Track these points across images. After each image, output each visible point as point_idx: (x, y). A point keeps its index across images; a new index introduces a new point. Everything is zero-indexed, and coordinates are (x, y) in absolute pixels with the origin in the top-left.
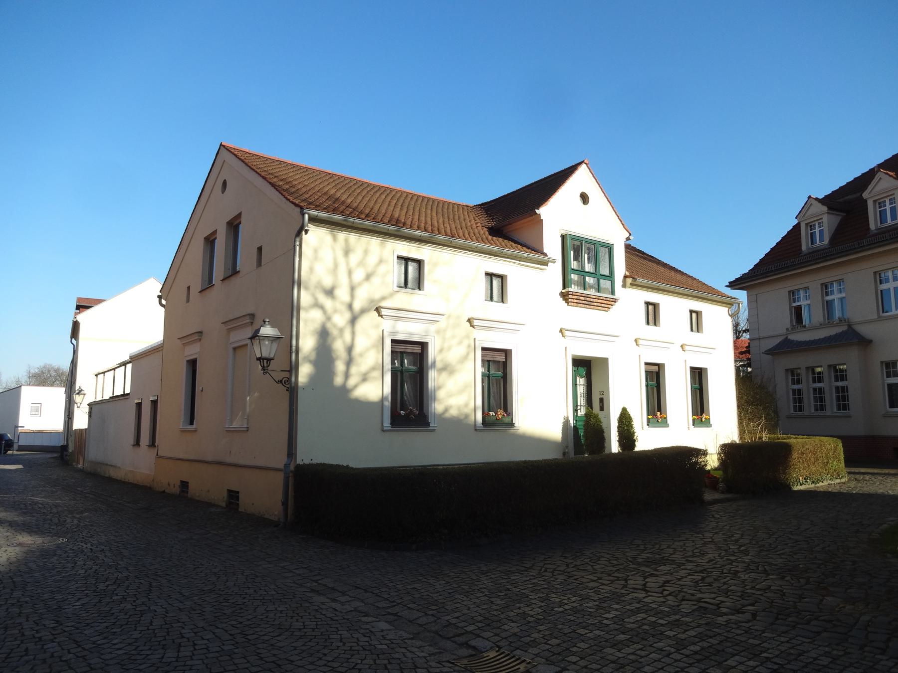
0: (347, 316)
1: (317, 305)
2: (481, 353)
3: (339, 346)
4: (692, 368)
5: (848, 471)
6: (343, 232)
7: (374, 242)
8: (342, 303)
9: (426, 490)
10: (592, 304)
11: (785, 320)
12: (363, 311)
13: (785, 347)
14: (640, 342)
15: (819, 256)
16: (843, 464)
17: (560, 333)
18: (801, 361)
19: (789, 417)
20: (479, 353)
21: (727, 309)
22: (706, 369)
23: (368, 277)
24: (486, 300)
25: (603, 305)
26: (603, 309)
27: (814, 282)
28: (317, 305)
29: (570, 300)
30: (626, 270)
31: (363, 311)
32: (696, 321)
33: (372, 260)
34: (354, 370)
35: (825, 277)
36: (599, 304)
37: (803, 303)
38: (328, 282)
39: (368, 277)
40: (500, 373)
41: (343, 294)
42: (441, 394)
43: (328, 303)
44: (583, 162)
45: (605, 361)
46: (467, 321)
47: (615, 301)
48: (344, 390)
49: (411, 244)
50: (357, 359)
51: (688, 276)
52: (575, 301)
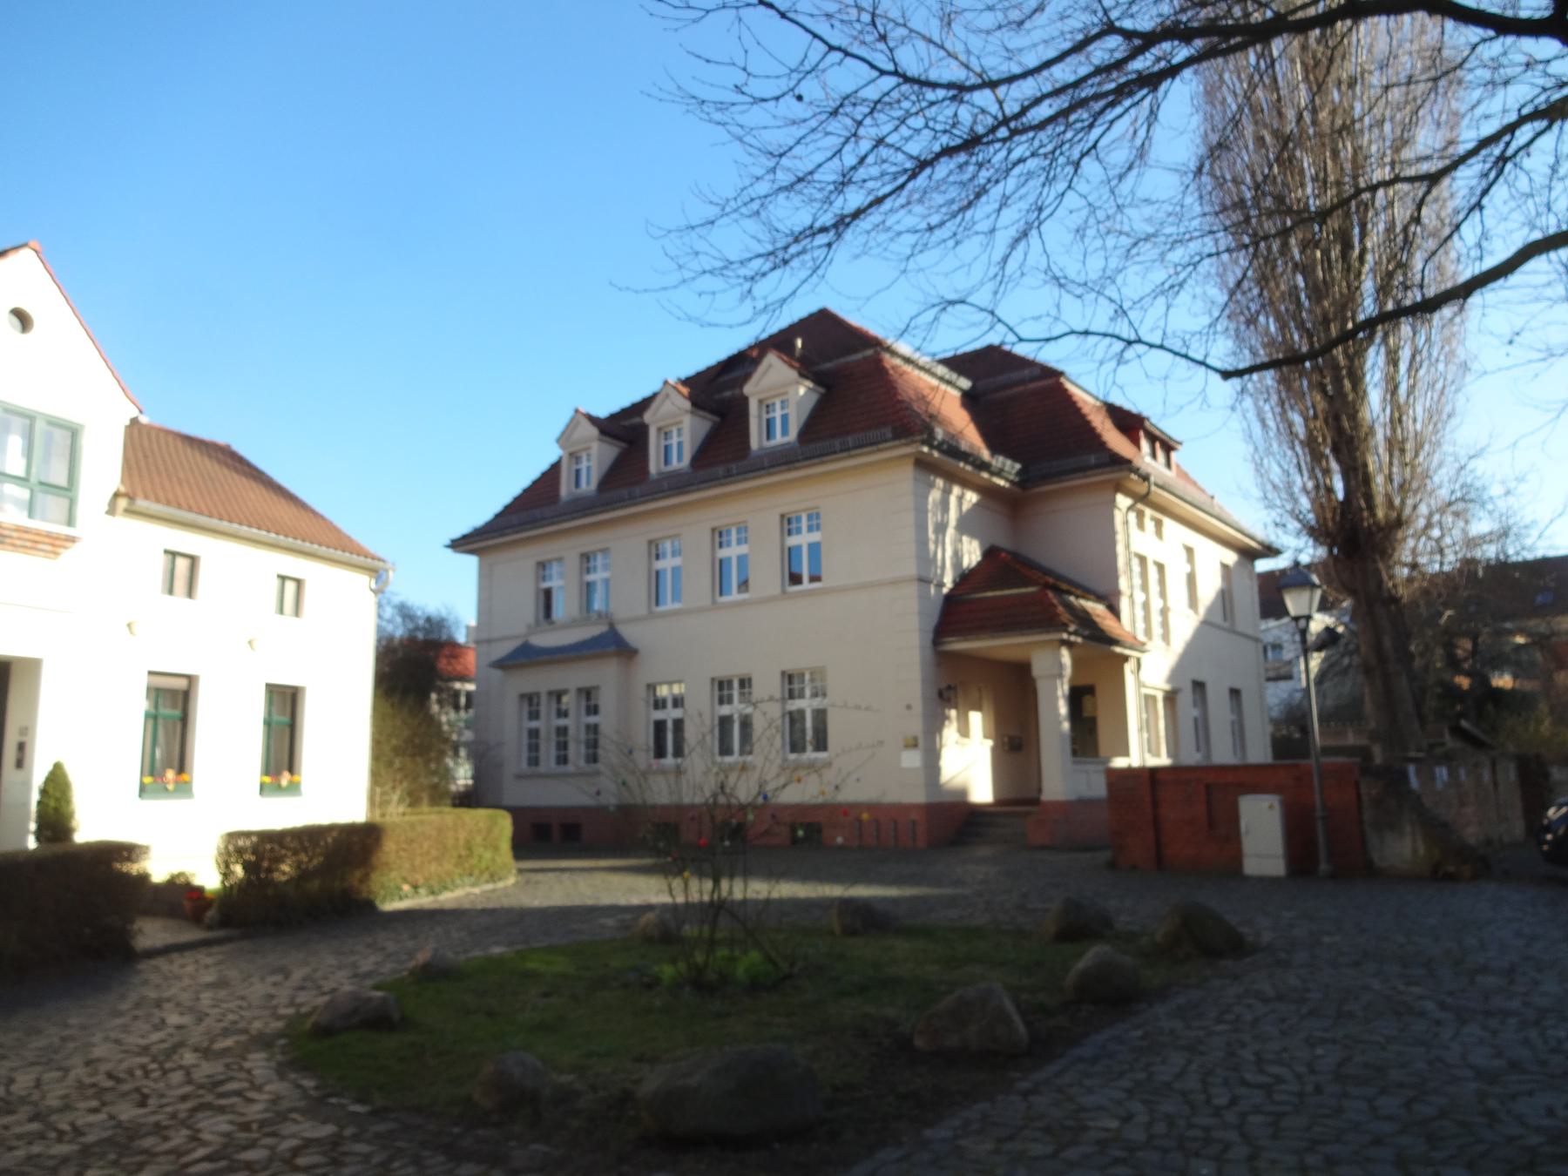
10: (40, 546)
11: (528, 609)
13: (524, 657)
15: (583, 507)
18: (541, 680)
19: (519, 777)
27: (567, 549)
30: (123, 482)
32: (292, 596)
35: (587, 542)
37: (554, 583)
40: (177, 713)
44: (25, 245)
47: (72, 540)
51: (313, 512)
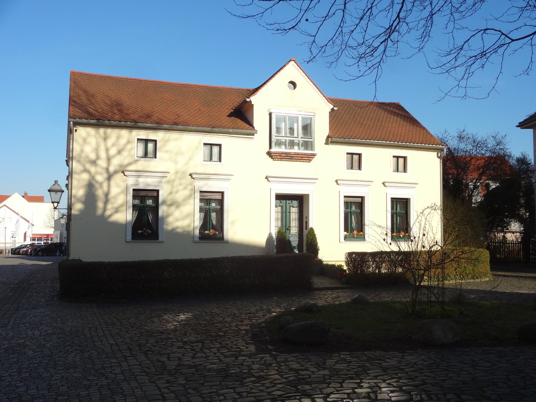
0: (105, 175)
1: (86, 171)
2: (199, 194)
3: (100, 193)
4: (392, 198)
5: (493, 273)
6: (123, 130)
7: (124, 133)
8: (102, 168)
9: (296, 280)
12: (116, 172)
14: (339, 182)
16: (488, 268)
17: (266, 179)
20: (198, 195)
21: (436, 153)
22: (410, 199)
23: (119, 152)
24: (204, 161)
25: (304, 158)
26: (305, 161)
28: (86, 171)
29: (273, 157)
31: (116, 172)
33: (123, 141)
34: (109, 206)
36: (300, 158)
38: (93, 156)
39: (119, 152)
41: (102, 163)
42: (170, 219)
43: (93, 170)
45: (308, 195)
46: (382, 184)
47: (314, 155)
48: (103, 219)
49: (146, 131)
50: (112, 201)
52: (279, 157)
